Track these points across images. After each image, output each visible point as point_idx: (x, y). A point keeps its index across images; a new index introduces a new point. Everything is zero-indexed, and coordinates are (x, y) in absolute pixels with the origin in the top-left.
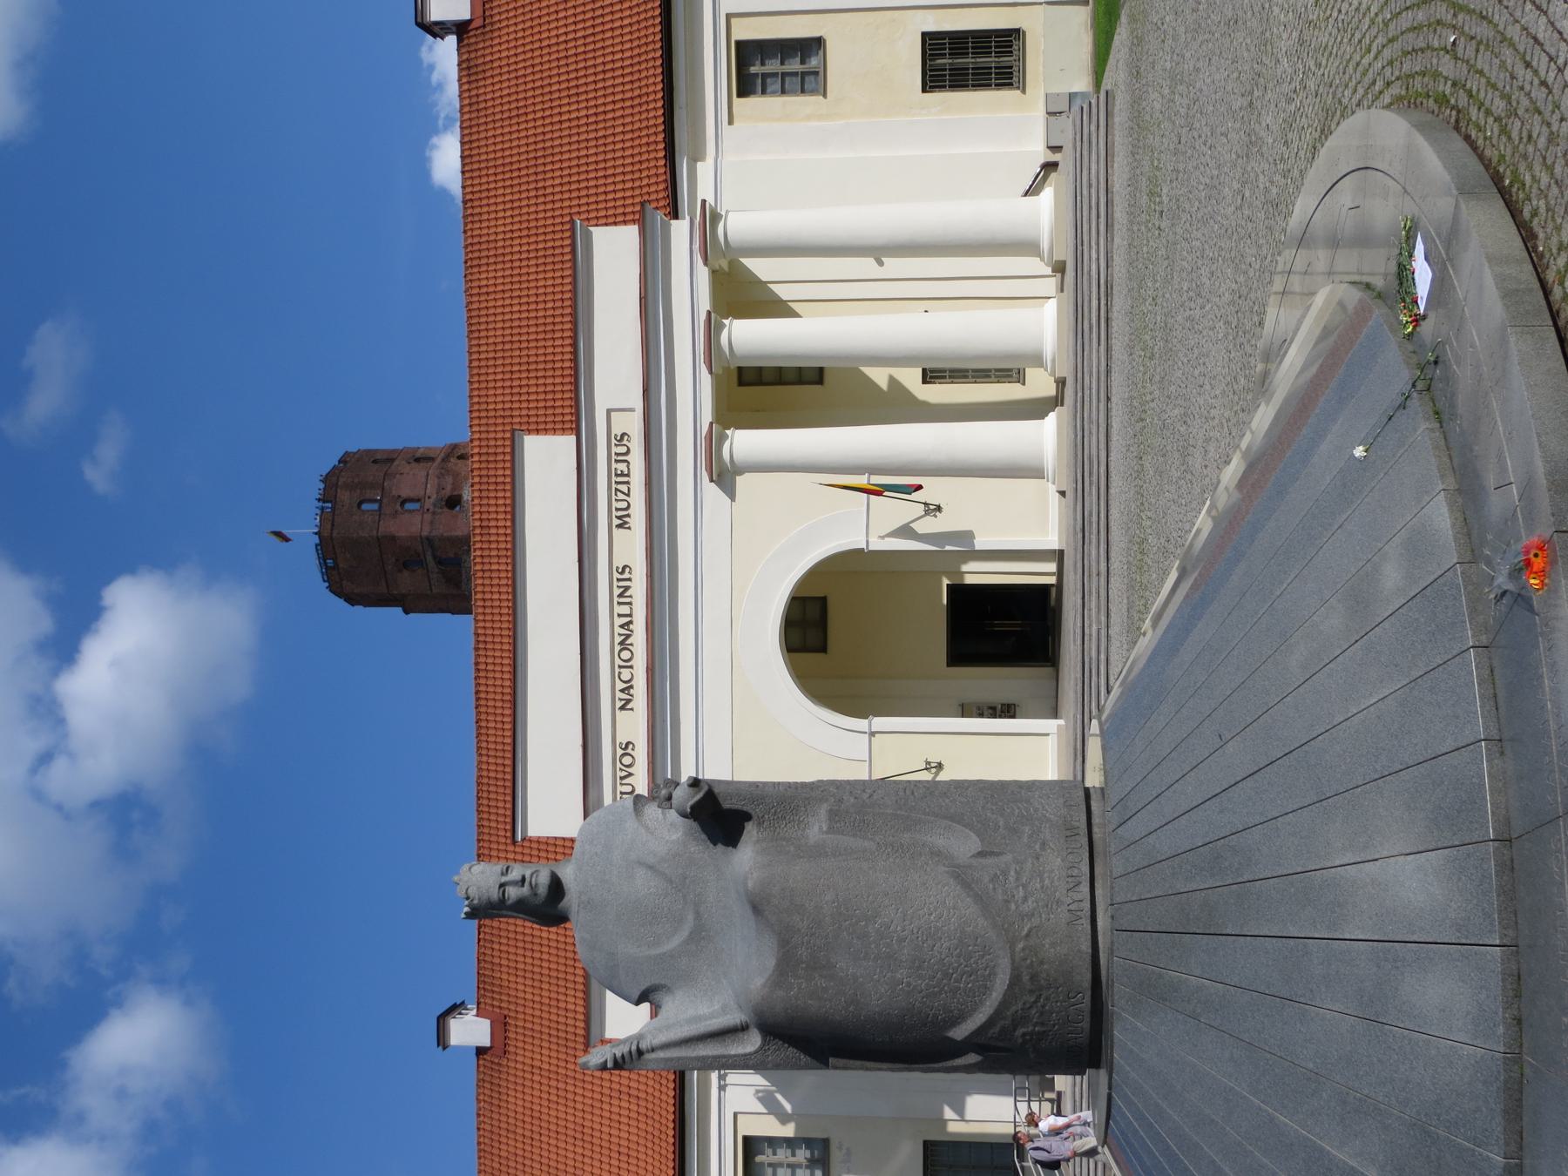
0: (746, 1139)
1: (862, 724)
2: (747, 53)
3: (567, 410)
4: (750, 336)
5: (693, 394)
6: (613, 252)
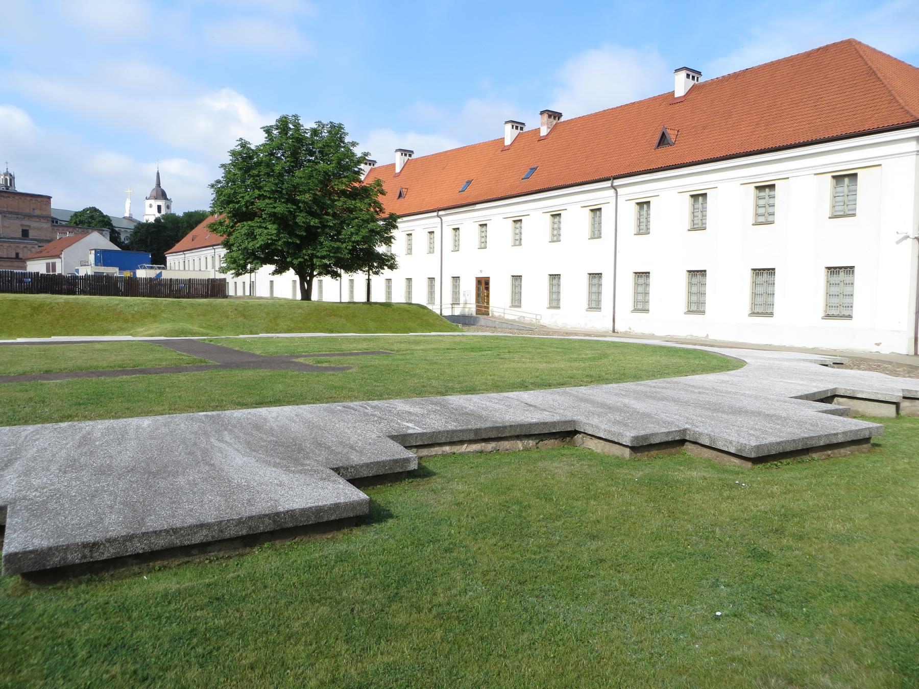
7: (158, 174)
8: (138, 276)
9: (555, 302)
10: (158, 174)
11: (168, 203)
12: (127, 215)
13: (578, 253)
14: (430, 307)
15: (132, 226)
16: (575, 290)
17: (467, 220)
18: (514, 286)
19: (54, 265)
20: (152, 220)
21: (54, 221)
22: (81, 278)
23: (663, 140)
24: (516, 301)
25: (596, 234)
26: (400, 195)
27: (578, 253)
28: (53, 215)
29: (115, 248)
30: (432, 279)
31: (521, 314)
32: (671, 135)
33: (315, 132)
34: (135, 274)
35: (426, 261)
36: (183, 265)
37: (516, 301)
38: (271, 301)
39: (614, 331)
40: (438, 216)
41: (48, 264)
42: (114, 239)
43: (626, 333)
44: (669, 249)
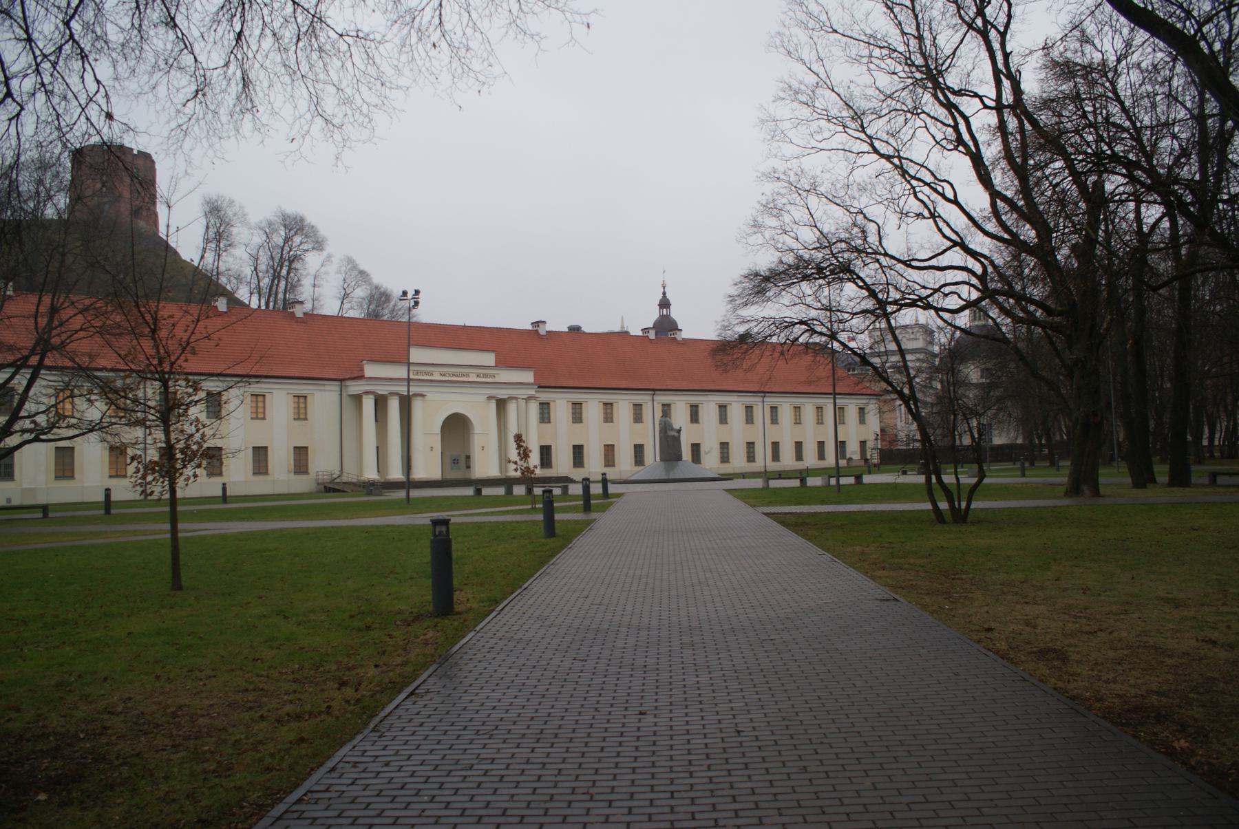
1: (439, 431)
2: (669, 405)
3: (502, 363)
4: (394, 406)
5: (503, 393)
6: (528, 377)
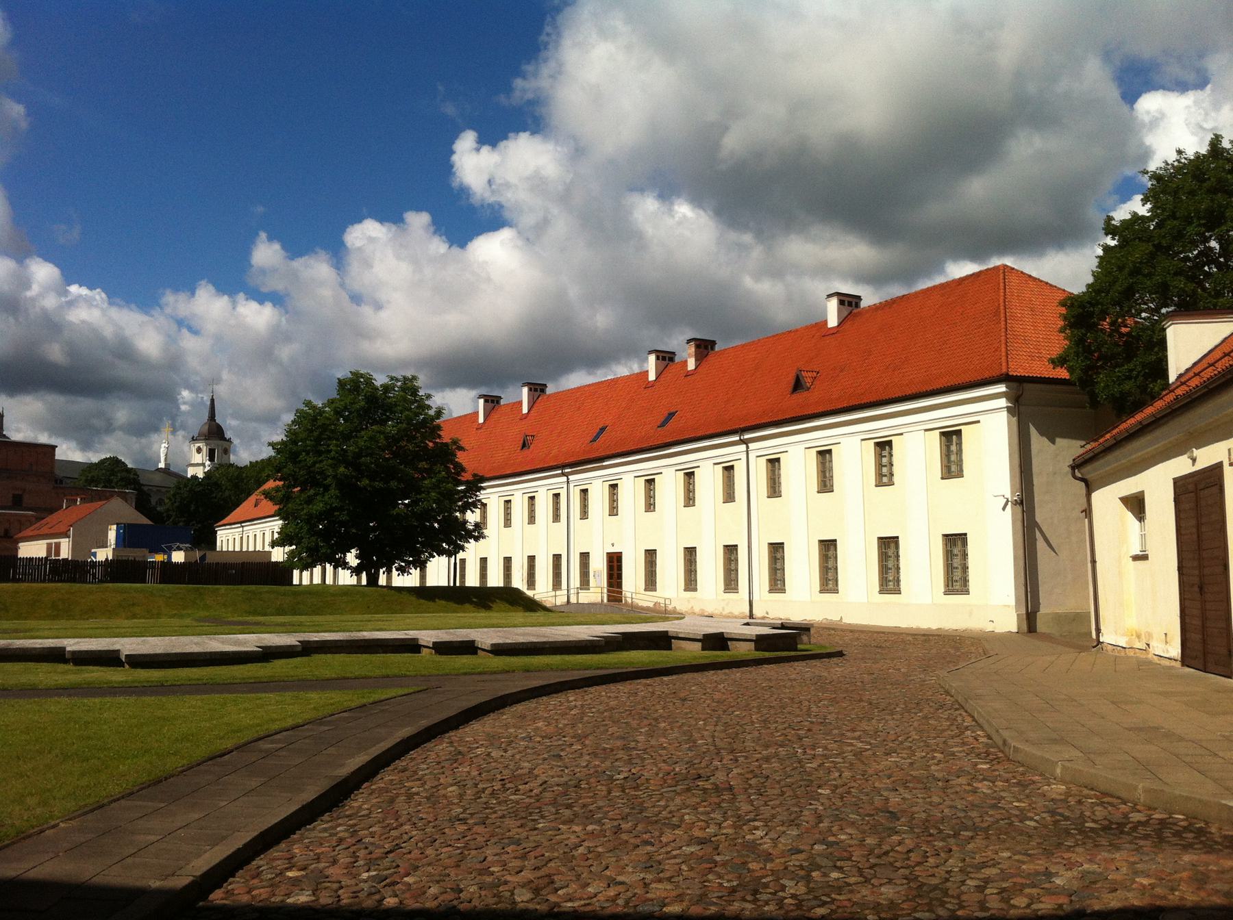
0: (960, 431)
7: (212, 400)
8: (174, 560)
9: (691, 582)
10: (212, 400)
11: (225, 444)
12: (162, 465)
13: (711, 525)
14: (530, 593)
15: (171, 483)
16: (857, 565)
17: (596, 481)
18: (949, 555)
19: (58, 546)
20: (277, 246)
21: (59, 481)
22: (100, 563)
23: (798, 385)
24: (651, 582)
25: (729, 497)
26: (524, 446)
27: (711, 525)
28: (59, 473)
29: (144, 520)
30: (731, 550)
31: (655, 600)
32: (807, 378)
33: (386, 388)
34: (170, 557)
35: (521, 535)
36: (251, 535)
37: (651, 582)
38: (1142, 656)
39: (751, 616)
40: (563, 474)
41: (49, 546)
42: (142, 504)
43: (764, 618)
44: (797, 518)
